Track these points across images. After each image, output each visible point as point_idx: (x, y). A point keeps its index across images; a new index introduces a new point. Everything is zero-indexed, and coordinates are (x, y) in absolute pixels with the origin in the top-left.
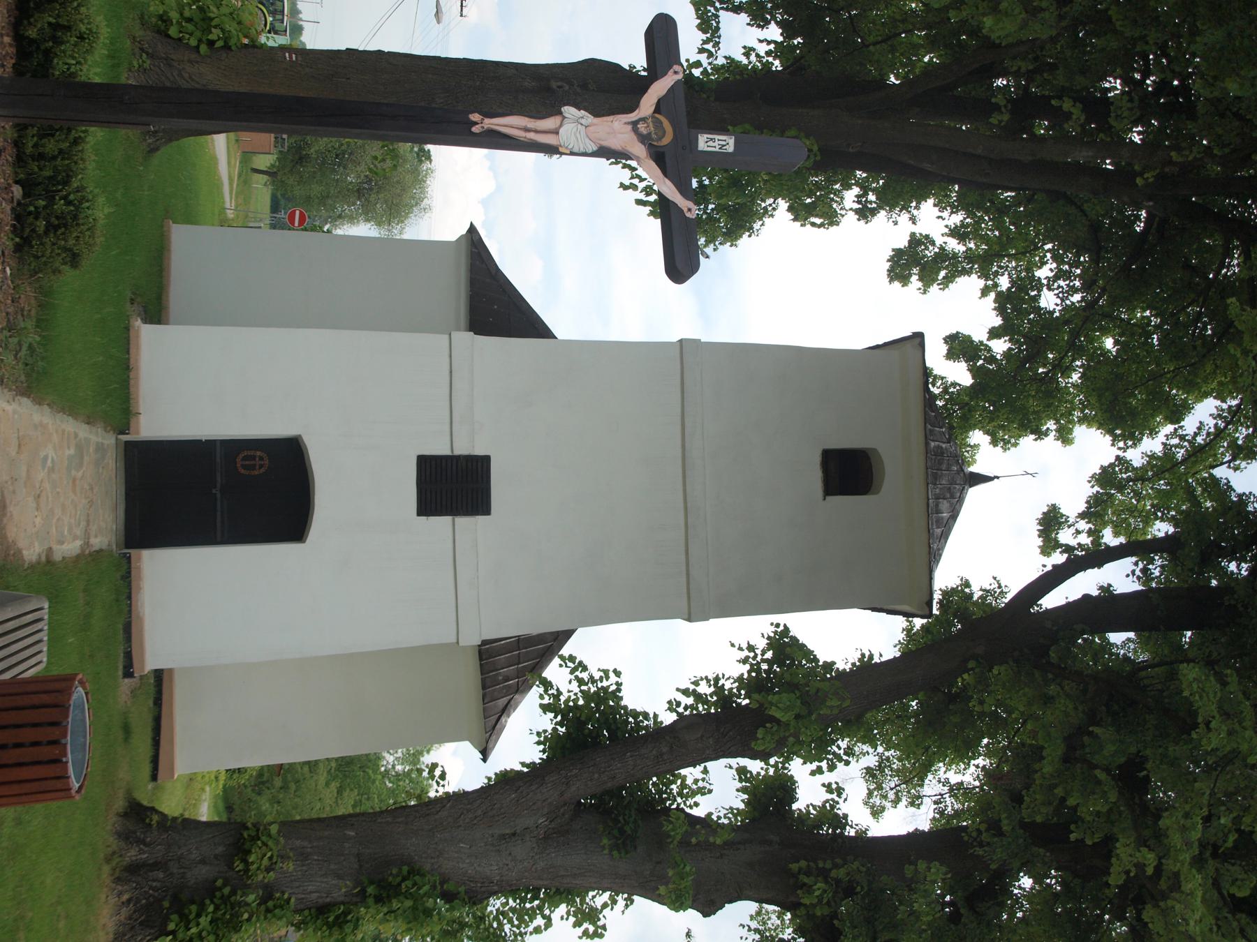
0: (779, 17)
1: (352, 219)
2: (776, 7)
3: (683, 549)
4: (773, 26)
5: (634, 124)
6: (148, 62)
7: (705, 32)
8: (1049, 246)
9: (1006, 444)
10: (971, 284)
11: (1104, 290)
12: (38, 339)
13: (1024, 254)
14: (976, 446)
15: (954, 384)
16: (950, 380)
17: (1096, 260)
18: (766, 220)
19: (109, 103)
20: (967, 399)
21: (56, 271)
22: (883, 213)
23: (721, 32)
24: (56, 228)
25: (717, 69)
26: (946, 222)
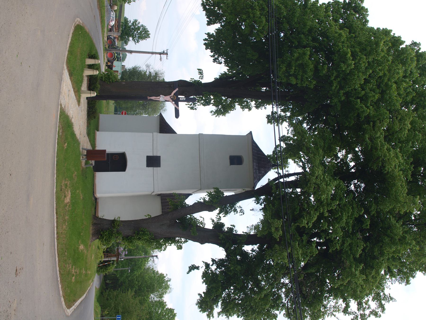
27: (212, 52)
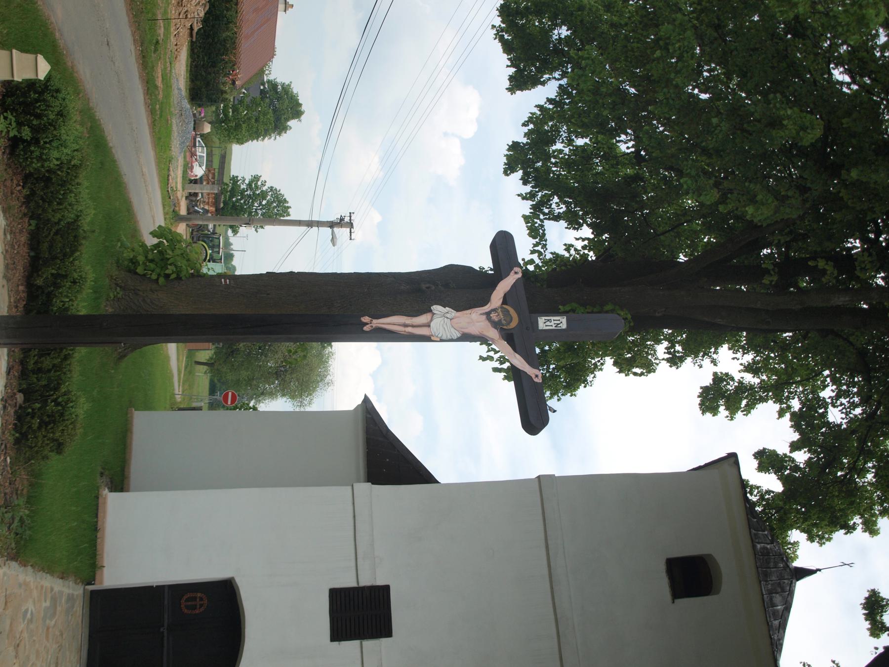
0: (589, 221)
1: (272, 395)
2: (586, 214)
3: (557, 656)
4: (585, 227)
5: (488, 314)
6: (121, 293)
7: (534, 238)
8: (827, 373)
9: (822, 540)
10: (770, 408)
11: (879, 404)
12: (27, 512)
13: (808, 380)
14: (796, 544)
15: (768, 492)
16: (764, 488)
17: (867, 379)
18: (597, 373)
19: (93, 329)
20: (781, 503)
21: (45, 458)
22: (689, 360)
23: (547, 237)
24: (47, 424)
25: (546, 262)
26: (740, 361)
27: (525, 183)
